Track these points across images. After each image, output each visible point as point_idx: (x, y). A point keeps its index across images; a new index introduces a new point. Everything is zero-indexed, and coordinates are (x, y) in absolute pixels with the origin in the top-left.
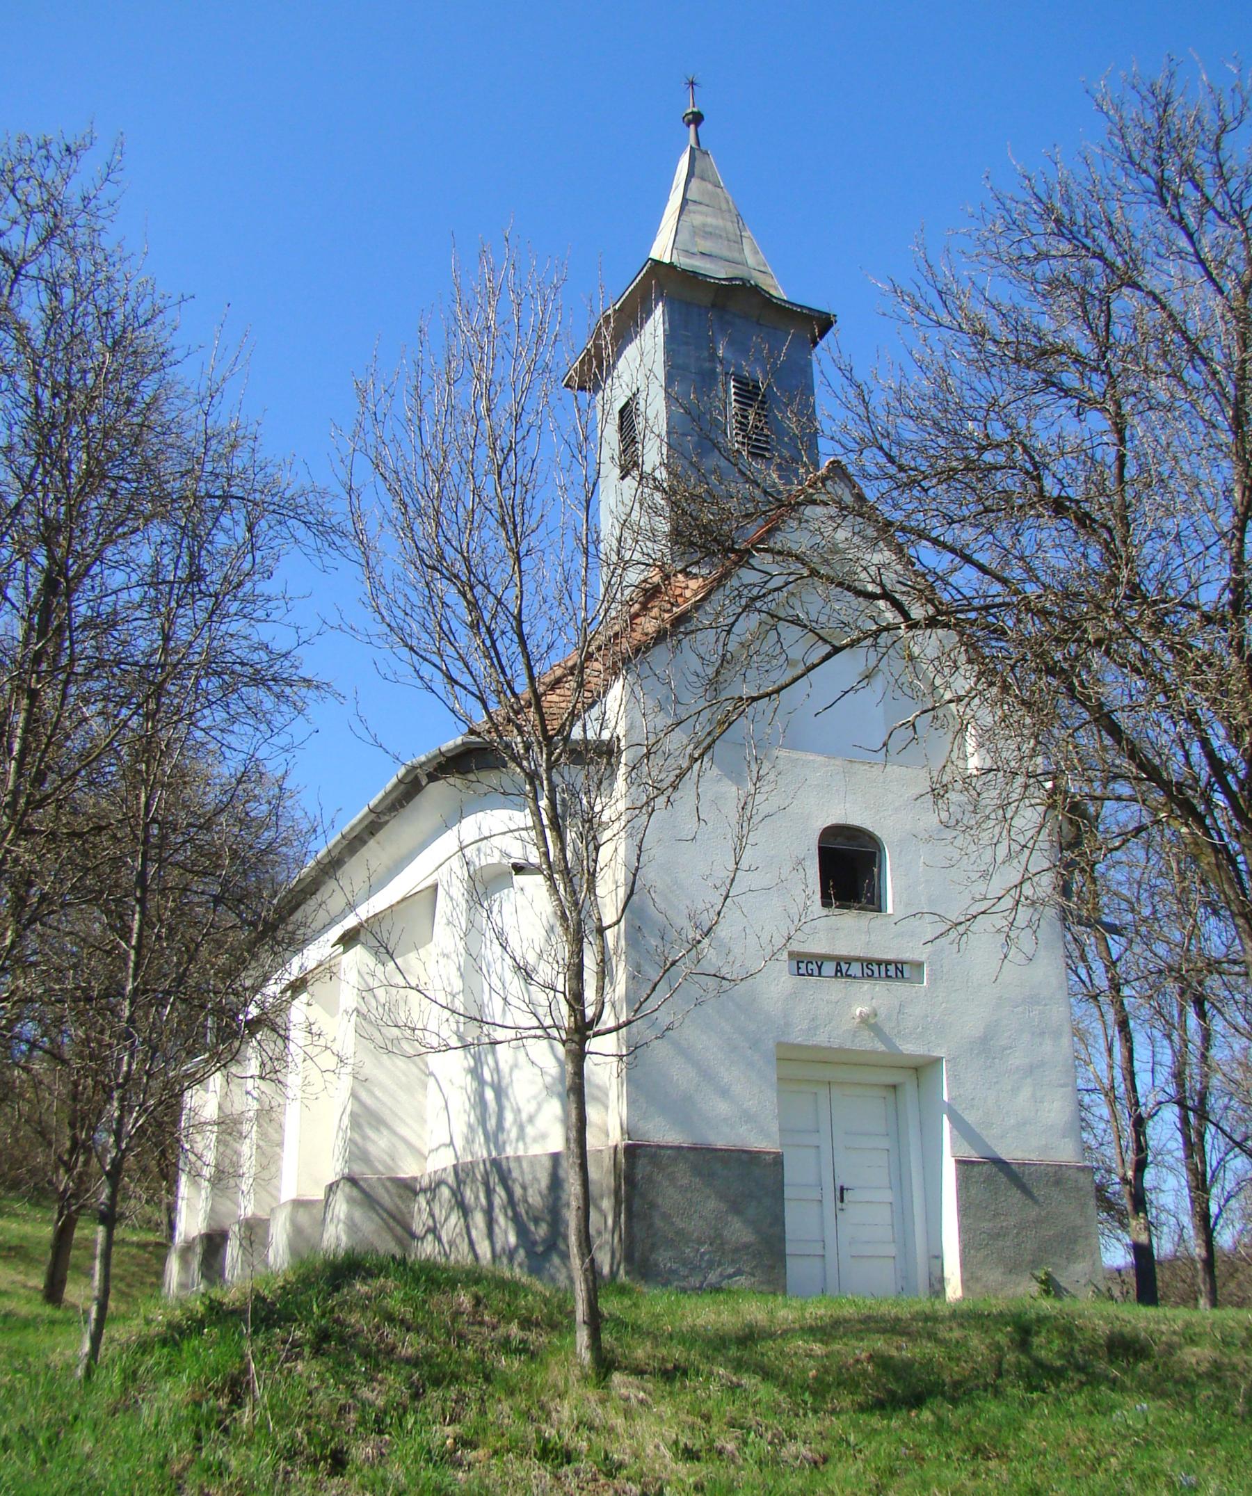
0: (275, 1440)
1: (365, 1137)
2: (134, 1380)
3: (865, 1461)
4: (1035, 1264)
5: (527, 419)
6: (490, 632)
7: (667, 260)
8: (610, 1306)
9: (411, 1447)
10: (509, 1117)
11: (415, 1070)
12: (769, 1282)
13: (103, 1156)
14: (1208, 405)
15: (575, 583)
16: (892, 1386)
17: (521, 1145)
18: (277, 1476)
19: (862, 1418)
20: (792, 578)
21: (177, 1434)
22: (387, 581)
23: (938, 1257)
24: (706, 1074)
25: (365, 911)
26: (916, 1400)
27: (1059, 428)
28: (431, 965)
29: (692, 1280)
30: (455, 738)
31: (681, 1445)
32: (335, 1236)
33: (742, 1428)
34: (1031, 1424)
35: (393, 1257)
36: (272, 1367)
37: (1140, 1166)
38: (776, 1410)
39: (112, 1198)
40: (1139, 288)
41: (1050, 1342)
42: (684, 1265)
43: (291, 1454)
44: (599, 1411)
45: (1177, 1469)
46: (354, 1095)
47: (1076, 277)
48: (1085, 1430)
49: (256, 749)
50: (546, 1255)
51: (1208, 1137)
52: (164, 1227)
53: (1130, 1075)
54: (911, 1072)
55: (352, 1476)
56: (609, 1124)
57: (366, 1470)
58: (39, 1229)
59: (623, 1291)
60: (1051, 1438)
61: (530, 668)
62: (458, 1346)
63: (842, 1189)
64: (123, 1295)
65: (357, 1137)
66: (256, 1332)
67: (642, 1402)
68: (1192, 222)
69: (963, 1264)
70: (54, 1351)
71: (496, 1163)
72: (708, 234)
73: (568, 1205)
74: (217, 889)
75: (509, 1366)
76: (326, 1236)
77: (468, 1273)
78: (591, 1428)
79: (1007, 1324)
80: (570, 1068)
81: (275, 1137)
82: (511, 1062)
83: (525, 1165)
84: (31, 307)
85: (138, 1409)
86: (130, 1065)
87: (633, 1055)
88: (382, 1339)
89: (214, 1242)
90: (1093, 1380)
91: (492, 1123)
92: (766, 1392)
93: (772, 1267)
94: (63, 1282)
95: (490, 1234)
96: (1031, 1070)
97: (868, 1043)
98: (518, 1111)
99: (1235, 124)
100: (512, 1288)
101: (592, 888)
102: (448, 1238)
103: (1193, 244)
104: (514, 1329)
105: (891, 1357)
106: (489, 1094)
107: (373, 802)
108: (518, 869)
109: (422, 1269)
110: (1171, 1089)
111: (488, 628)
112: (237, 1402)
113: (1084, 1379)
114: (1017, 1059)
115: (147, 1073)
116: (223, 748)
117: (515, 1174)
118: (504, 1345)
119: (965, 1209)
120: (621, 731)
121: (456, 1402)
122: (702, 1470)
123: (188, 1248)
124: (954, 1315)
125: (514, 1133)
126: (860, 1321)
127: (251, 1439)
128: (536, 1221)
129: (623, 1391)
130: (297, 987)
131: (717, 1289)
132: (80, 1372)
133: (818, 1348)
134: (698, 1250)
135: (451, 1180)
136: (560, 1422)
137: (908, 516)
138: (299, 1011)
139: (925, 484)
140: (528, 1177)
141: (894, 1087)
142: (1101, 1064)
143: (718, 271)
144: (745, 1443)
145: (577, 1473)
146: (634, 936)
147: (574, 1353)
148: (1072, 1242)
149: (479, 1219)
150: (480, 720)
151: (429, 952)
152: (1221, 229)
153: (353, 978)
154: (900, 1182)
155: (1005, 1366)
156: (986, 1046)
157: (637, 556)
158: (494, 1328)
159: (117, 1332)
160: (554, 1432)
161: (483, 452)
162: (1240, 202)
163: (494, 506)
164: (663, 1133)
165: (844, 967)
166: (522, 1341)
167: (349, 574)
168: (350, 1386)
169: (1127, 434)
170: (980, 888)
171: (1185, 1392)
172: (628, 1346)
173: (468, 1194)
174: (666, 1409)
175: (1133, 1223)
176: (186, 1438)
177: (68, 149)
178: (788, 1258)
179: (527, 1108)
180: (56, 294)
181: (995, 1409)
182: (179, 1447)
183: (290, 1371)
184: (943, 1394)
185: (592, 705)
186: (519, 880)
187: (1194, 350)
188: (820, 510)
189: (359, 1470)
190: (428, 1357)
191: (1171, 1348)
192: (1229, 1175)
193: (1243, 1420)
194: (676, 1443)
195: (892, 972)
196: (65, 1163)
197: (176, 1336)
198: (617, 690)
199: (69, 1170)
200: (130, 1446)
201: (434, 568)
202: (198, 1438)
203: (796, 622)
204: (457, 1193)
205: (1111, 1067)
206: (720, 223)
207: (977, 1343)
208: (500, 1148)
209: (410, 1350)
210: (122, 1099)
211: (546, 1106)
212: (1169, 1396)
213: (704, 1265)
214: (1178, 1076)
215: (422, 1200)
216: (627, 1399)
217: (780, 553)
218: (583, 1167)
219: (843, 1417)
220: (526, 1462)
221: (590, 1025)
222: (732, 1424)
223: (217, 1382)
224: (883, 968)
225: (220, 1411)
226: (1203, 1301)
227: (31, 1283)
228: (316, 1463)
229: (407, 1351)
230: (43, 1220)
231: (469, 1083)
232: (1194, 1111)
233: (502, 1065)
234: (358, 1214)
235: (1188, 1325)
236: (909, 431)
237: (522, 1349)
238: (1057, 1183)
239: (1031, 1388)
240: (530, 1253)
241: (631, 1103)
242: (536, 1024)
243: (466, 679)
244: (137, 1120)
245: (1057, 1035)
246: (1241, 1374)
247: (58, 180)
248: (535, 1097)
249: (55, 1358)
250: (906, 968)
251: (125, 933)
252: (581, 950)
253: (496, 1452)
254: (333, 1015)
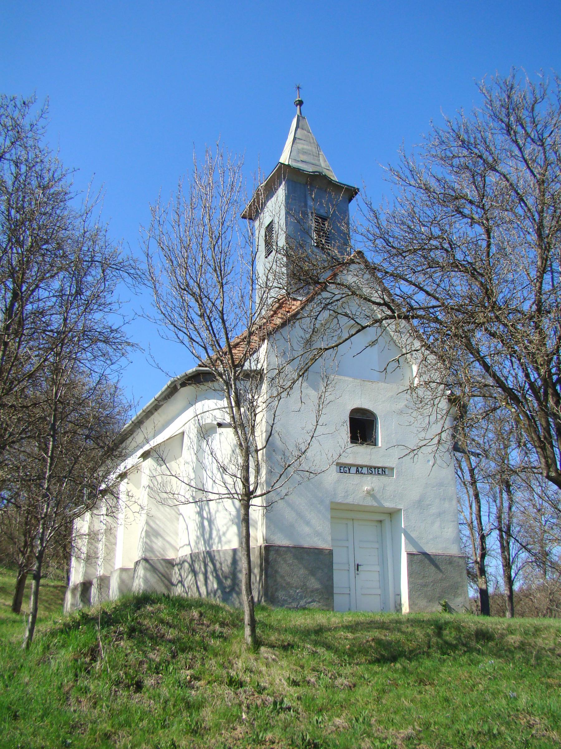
0: (110, 676)
1: (151, 541)
2: (48, 649)
3: (372, 686)
4: (440, 598)
5: (226, 224)
6: (209, 318)
7: (287, 163)
8: (259, 616)
9: (171, 680)
10: (214, 533)
11: (173, 512)
12: (326, 605)
13: (38, 549)
14: (528, 223)
15: (246, 299)
16: (383, 653)
17: (219, 545)
18: (111, 693)
19: (370, 666)
20: (344, 296)
21: (67, 673)
22: (164, 294)
23: (399, 595)
24: (300, 515)
25: (153, 443)
26: (394, 659)
27: (462, 230)
28: (182, 466)
29: (293, 604)
30: (192, 368)
31: (291, 679)
32: (138, 585)
33: (318, 671)
34: (444, 669)
35: (164, 595)
36: (109, 644)
37: (483, 556)
38: (332, 663)
39: (39, 568)
40: (497, 172)
41: (451, 633)
42: (290, 598)
43: (118, 683)
44: (255, 664)
45: (508, 690)
46: (147, 523)
47: (471, 166)
48: (467, 672)
49: (105, 370)
50: (230, 593)
51: (511, 544)
52: (65, 579)
53: (479, 517)
55: (145, 693)
56: (258, 536)
57: (151, 690)
58: (10, 580)
59: (263, 609)
60: (453, 676)
61: (227, 334)
62: (192, 634)
63: (358, 565)
64: (48, 609)
65: (148, 541)
66: (103, 628)
67: (274, 660)
68: (521, 142)
69: (410, 598)
70: (13, 636)
71: (208, 553)
72: (305, 153)
73: (241, 571)
74: (87, 432)
75: (215, 644)
76: (135, 584)
77: (197, 602)
78: (251, 671)
79: (432, 625)
80: (242, 511)
81: (113, 541)
82: (215, 509)
83: (221, 554)
84: (7, 171)
85: (50, 663)
86: (47, 509)
87: (268, 507)
88: (158, 631)
89: (86, 586)
90: (470, 650)
91: (207, 536)
92: (328, 655)
93: (328, 599)
94: (21, 603)
95: (206, 584)
96: (439, 514)
97: (370, 502)
98: (218, 530)
99: (540, 100)
100: (216, 608)
101: (253, 433)
102: (189, 586)
103: (521, 152)
104: (217, 626)
105: (382, 640)
106: (206, 523)
107: (157, 396)
108: (220, 425)
109: (176, 600)
110: (496, 524)
111: (208, 317)
112: (94, 659)
113: (466, 649)
114: (433, 510)
115: (55, 512)
116: (90, 369)
117: (217, 558)
118: (213, 634)
119: (410, 574)
120: (265, 367)
121: (191, 660)
122: (300, 691)
123: (75, 588)
124: (408, 620)
125: (216, 540)
126: (367, 623)
127: (99, 676)
128: (226, 578)
129: (266, 655)
130: (123, 476)
131: (304, 608)
132: (24, 645)
133: (350, 635)
135: (189, 560)
136: (238, 669)
137: (396, 269)
138: (123, 486)
139: (404, 254)
140: (223, 559)
141: (381, 521)
142: (467, 512)
143: (309, 169)
144: (319, 678)
145: (245, 692)
146: (269, 457)
147: (244, 638)
148: (456, 589)
149: (201, 577)
150: (205, 358)
151: (181, 460)
152: (533, 146)
153: (148, 472)
154: (383, 562)
155: (432, 644)
156: (420, 504)
157: (275, 284)
158: (208, 626)
159: (41, 627)
160: (235, 673)
161: (207, 239)
162: (542, 135)
163: (212, 263)
164: (281, 541)
165: (360, 469)
166: (221, 632)
167: (147, 292)
168: (144, 652)
169: (492, 235)
170: (423, 435)
171: (510, 656)
172: (268, 634)
173: (197, 566)
174: (284, 663)
175: (480, 580)
176: (71, 676)
177: (24, 103)
178: (335, 595)
179: (223, 529)
180: (18, 166)
181: (428, 663)
182: (67, 680)
183: (118, 645)
184: (405, 656)
185: (253, 354)
186: (220, 430)
187: (521, 200)
188: (356, 266)
189: (148, 690)
190: (179, 639)
191: (502, 636)
192: (520, 560)
193: (535, 668)
194: (289, 678)
195: (380, 472)
196: (22, 552)
197: (68, 629)
198: (265, 346)
199: (24, 555)
200: (45, 679)
201: (185, 290)
202: (76, 675)
203: (346, 315)
204: (192, 566)
205: (471, 514)
206: (309, 148)
207: (419, 633)
208: (211, 547)
209: (171, 636)
210: (43, 524)
211: (230, 529)
212: (503, 657)
214: (499, 518)
215: (176, 568)
216: (267, 658)
217: (339, 284)
218: (248, 555)
219: (362, 667)
220: (223, 686)
221: (252, 493)
222: (313, 670)
223: (85, 650)
225: (86, 663)
226: (508, 614)
227: (7, 603)
228: (129, 687)
229: (170, 637)
230: (13, 576)
231: (197, 518)
232: (505, 533)
233: (211, 510)
234: (149, 575)
235: (509, 626)
236: (397, 231)
237: (221, 636)
238: (450, 563)
239: (443, 653)
240: (223, 592)
241: (268, 527)
242: (226, 492)
243: (198, 339)
244: (50, 533)
245: (451, 500)
246: (533, 647)
247: (21, 117)
248: (226, 524)
249: (13, 639)
251: (46, 451)
252: (248, 459)
253: (209, 682)
254: (138, 488)
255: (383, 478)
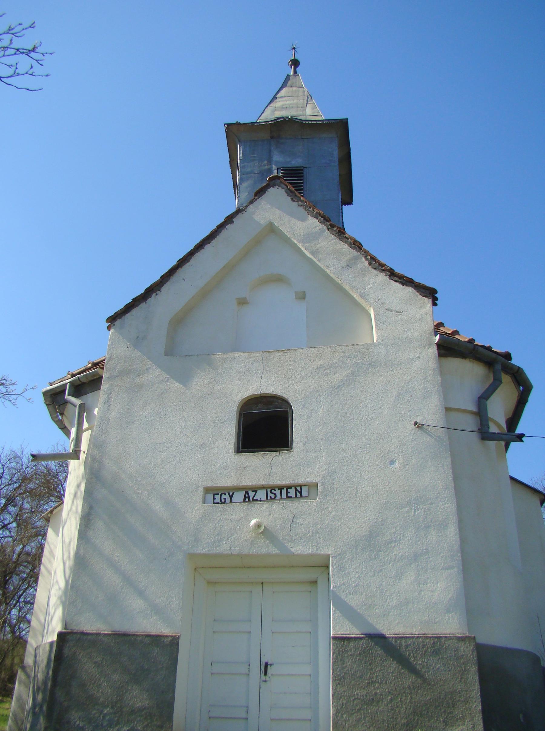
54: (325, 568)
63: (266, 665)
96: (416, 557)
97: (264, 548)
134: (102, 711)
156: (372, 542)
164: (90, 624)
165: (251, 494)
213: (105, 724)
224: (284, 491)
238: (436, 652)
250: (304, 490)
255: (295, 505)
